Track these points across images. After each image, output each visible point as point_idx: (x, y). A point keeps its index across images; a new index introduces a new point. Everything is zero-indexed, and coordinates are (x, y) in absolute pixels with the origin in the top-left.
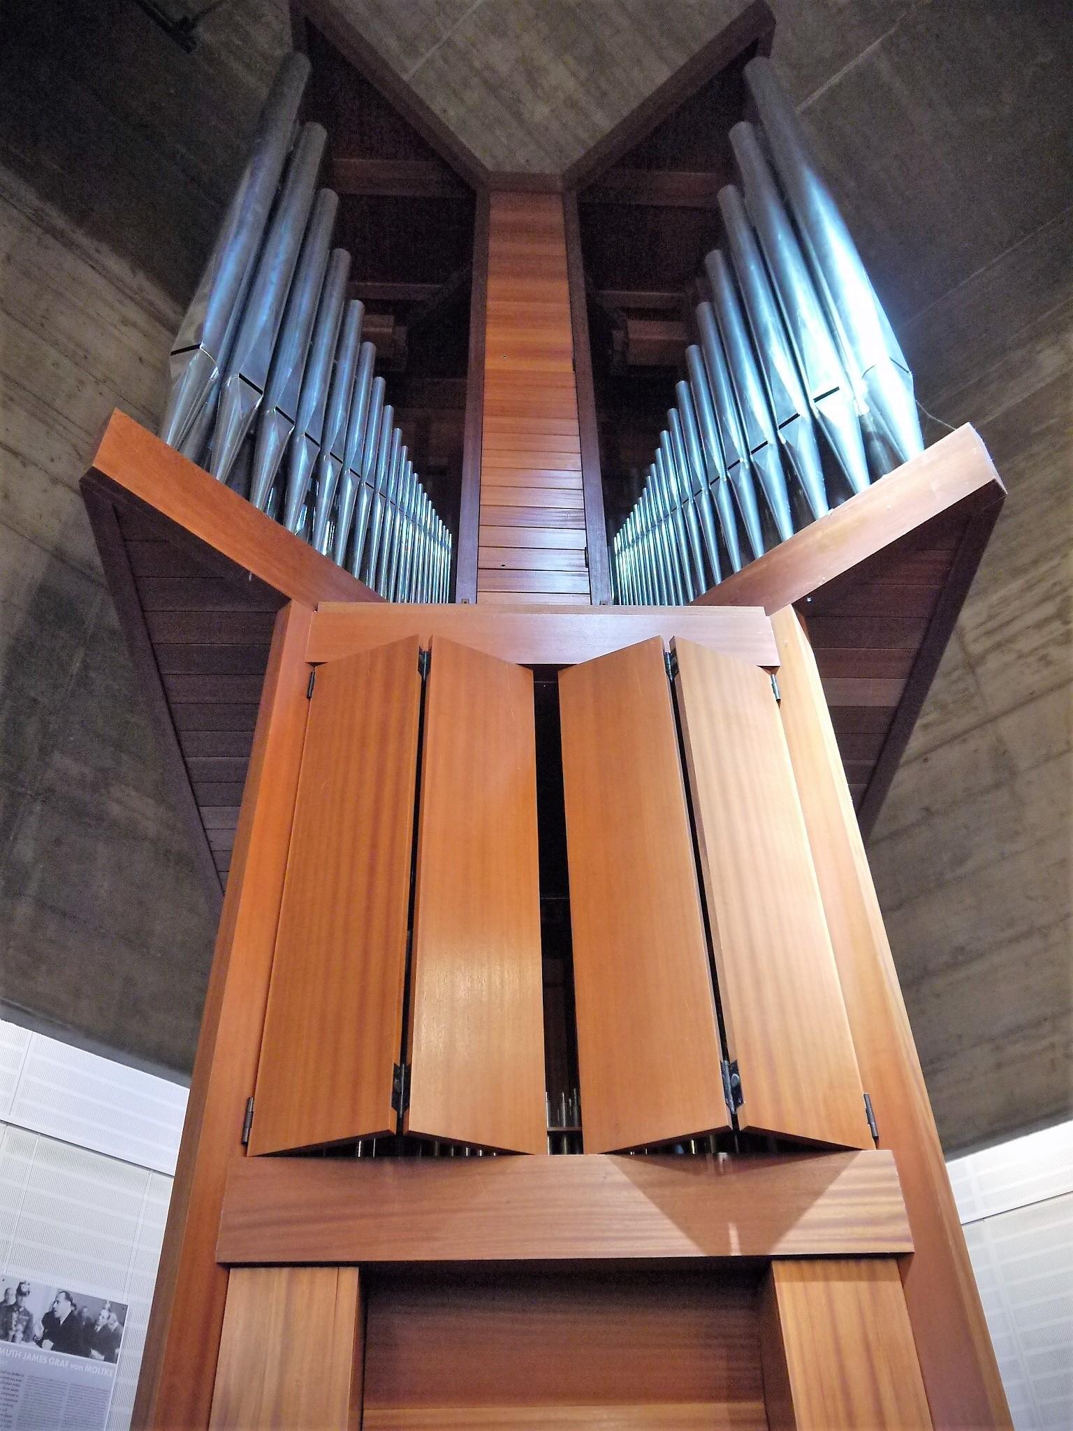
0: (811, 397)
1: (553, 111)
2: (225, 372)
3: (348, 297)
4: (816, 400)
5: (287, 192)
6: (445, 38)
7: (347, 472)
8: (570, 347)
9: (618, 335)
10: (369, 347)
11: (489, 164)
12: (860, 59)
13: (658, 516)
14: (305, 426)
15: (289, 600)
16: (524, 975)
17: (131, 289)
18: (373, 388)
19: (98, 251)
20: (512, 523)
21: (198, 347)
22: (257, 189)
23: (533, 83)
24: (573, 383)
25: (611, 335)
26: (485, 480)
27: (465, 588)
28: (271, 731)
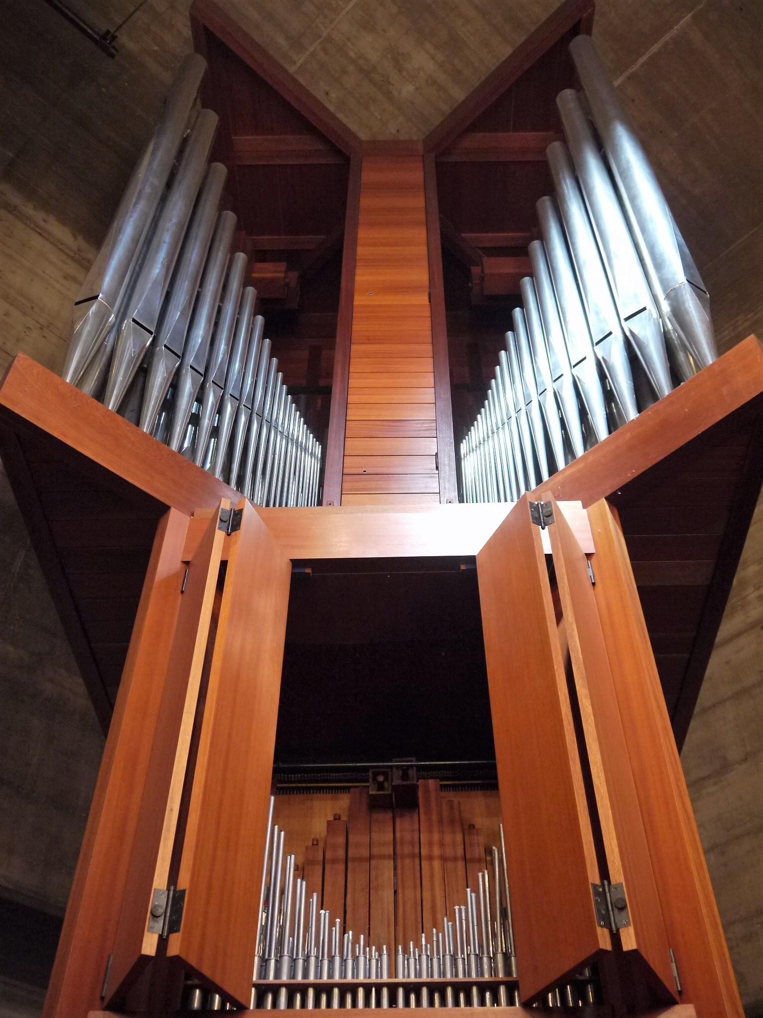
0: (622, 317)
1: (417, 89)
2: (122, 315)
3: (234, 249)
4: (627, 319)
5: (181, 169)
6: (325, 34)
7: (227, 397)
8: (427, 283)
9: (475, 270)
10: (251, 291)
11: (363, 135)
12: (675, 31)
13: (497, 424)
14: (190, 360)
15: (168, 508)
16: (344, 838)
17: (71, 250)
18: (253, 325)
19: (45, 221)
20: (374, 434)
21: (96, 297)
22: (155, 166)
23: (400, 69)
24: (428, 314)
25: (470, 270)
26: (351, 399)
27: (332, 490)
28: (147, 623)
